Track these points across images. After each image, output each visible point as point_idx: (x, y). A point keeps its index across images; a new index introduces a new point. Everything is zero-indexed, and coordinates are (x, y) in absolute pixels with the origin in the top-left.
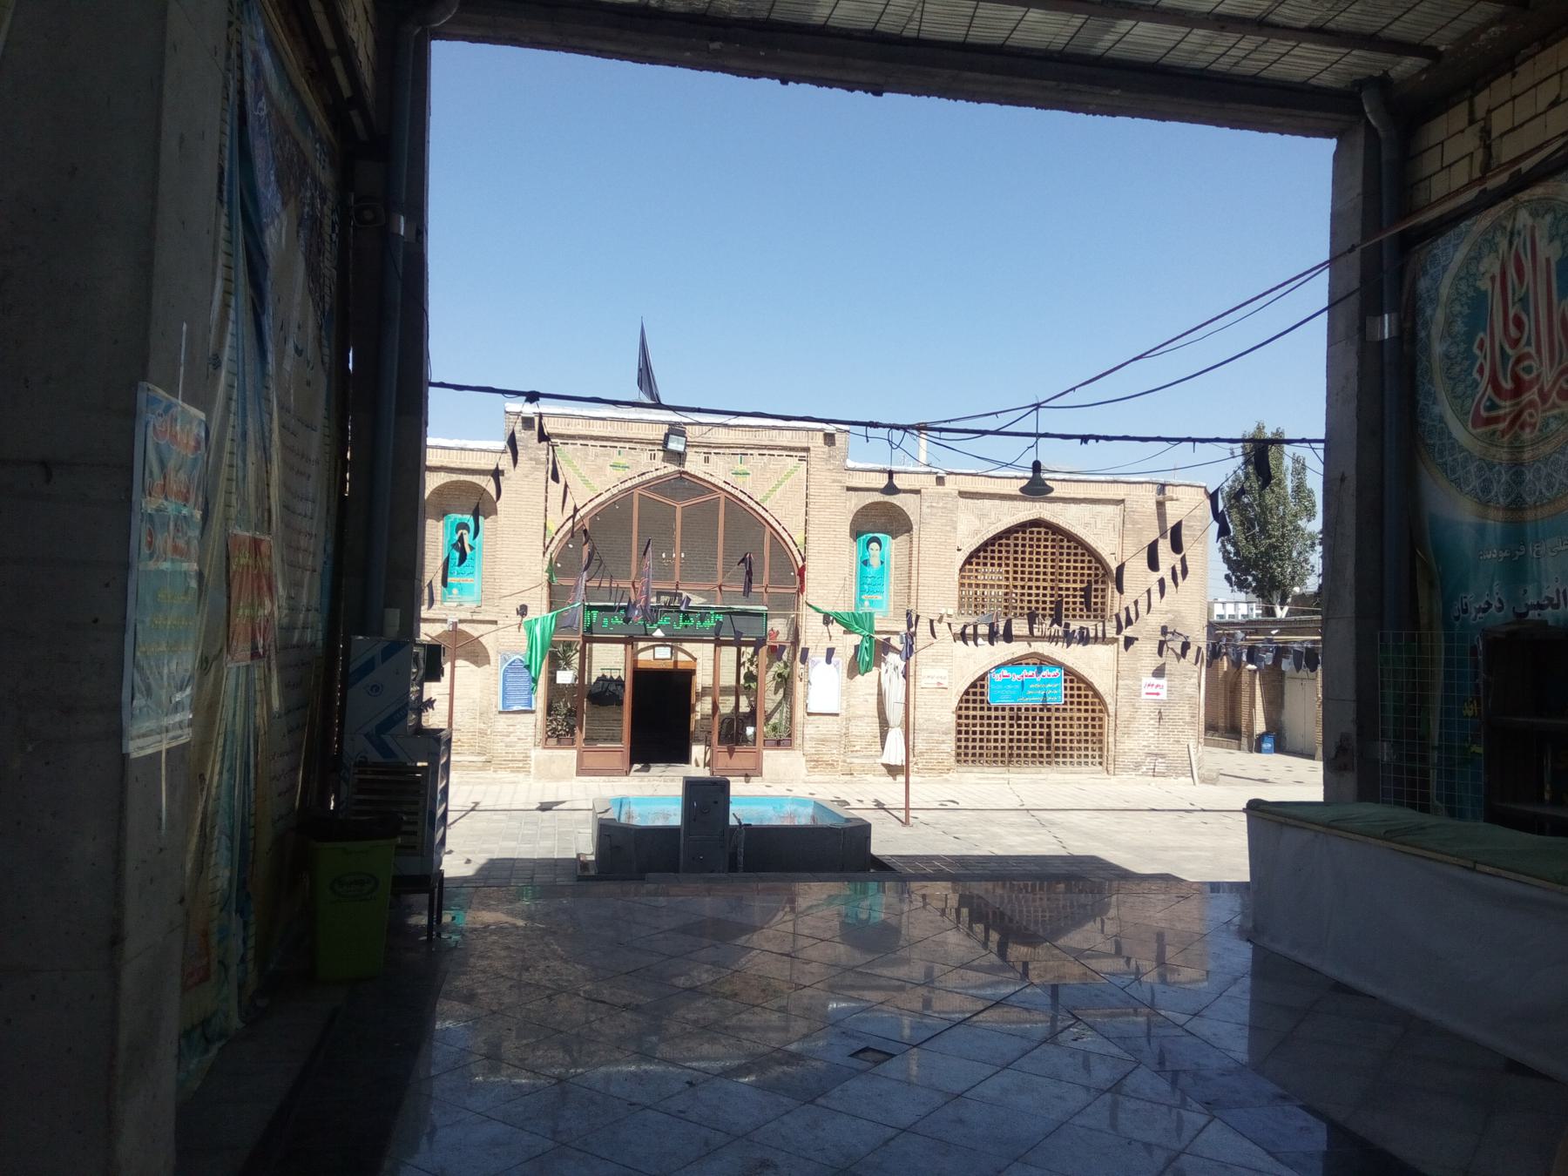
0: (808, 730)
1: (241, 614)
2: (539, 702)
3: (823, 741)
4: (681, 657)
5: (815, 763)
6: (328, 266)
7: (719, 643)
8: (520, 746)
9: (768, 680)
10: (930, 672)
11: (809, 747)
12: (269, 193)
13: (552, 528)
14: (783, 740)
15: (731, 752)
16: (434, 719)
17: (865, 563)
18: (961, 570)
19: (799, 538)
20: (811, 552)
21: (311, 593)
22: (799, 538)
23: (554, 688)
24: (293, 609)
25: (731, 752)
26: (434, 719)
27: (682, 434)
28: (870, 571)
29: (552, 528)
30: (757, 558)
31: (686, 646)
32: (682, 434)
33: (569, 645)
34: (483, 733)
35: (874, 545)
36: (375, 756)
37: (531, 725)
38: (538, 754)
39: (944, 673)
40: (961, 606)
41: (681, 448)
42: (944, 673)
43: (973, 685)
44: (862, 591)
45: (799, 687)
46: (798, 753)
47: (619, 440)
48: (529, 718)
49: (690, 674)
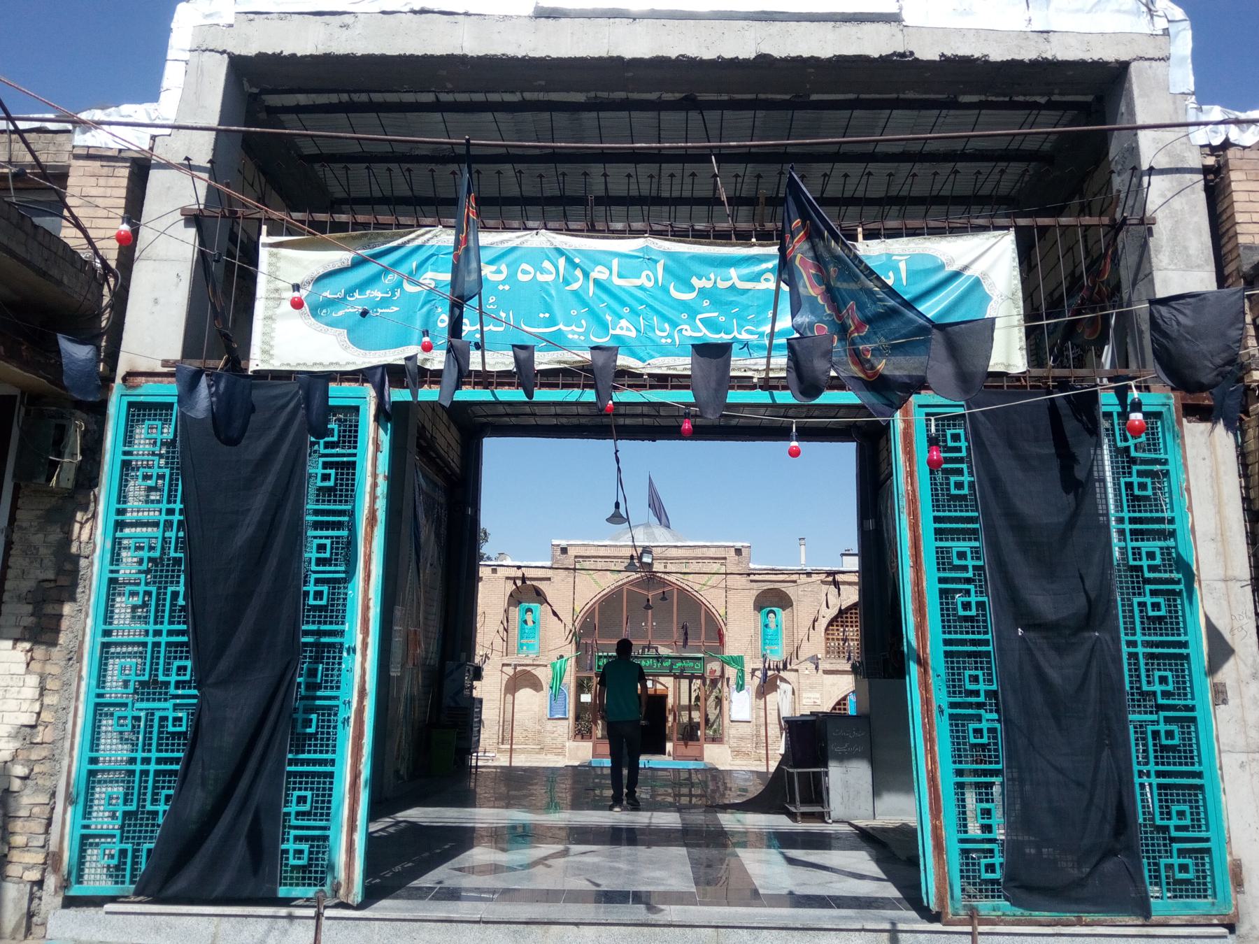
0: (731, 732)
1: (411, 652)
2: (571, 714)
3: (741, 739)
4: (659, 686)
5: (737, 753)
6: (443, 530)
7: (676, 677)
8: (560, 740)
9: (711, 701)
10: (810, 695)
11: (733, 742)
12: (422, 519)
13: (578, 609)
14: (717, 739)
15: (686, 745)
16: (475, 694)
17: (766, 626)
18: (827, 629)
19: (722, 612)
20: (729, 620)
21: (434, 647)
22: (722, 612)
23: (580, 706)
24: (427, 652)
25: (686, 745)
26: (475, 694)
27: (650, 553)
28: (769, 631)
29: (578, 609)
30: (699, 625)
31: (662, 679)
32: (650, 553)
33: (590, 679)
34: (540, 732)
35: (771, 615)
36: (452, 704)
37: (565, 727)
38: (570, 744)
39: (818, 695)
40: (828, 652)
41: (649, 561)
42: (818, 695)
43: (838, 703)
44: (522, 638)
45: (725, 703)
46: (726, 746)
47: (615, 557)
48: (565, 722)
49: (664, 697)
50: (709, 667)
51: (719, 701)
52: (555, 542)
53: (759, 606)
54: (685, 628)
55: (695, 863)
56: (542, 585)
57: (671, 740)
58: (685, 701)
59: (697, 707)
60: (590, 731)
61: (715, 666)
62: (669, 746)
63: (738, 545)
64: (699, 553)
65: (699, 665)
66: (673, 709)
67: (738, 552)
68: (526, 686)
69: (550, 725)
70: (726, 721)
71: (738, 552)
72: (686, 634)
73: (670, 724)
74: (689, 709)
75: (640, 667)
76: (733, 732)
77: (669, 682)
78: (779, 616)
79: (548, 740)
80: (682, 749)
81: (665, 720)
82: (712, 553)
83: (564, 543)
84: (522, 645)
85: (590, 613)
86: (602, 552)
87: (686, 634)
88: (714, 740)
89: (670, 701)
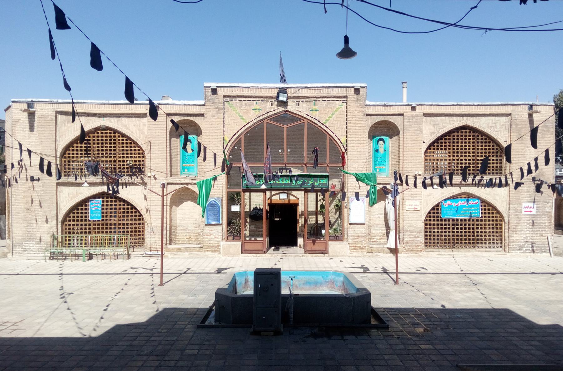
0: (350, 232)
2: (224, 221)
3: (358, 237)
4: (292, 198)
7: (307, 191)
8: (215, 240)
9: (331, 209)
13: (227, 139)
14: (338, 236)
17: (377, 151)
18: (425, 152)
19: (343, 140)
20: (349, 146)
22: (343, 140)
25: (314, 242)
27: (285, 92)
29: (227, 139)
30: (322, 150)
31: (294, 193)
32: (285, 92)
35: (381, 142)
39: (418, 203)
41: (285, 99)
42: (418, 203)
43: (433, 209)
44: (183, 163)
45: (345, 211)
46: (346, 243)
47: (256, 97)
48: (219, 228)
50: (331, 183)
51: (339, 209)
52: (206, 84)
53: (372, 136)
54: (315, 151)
55: (300, 217)
56: (197, 120)
57: (300, 236)
58: (312, 208)
59: (322, 213)
60: (239, 233)
61: (335, 183)
62: (300, 241)
63: (357, 85)
64: (325, 92)
65: (324, 181)
66: (303, 213)
67: (357, 91)
68: (188, 200)
69: (207, 229)
70: (346, 224)
71: (357, 91)
72: (316, 157)
73: (300, 225)
74: (316, 213)
75: (254, 209)
76: (351, 232)
77: (300, 195)
78: (387, 143)
79: (206, 241)
80: (310, 246)
81: (296, 222)
82: (335, 92)
83: (214, 85)
84: (183, 168)
85: (238, 143)
86: (246, 92)
87: (316, 157)
88: (336, 238)
89: (301, 208)
